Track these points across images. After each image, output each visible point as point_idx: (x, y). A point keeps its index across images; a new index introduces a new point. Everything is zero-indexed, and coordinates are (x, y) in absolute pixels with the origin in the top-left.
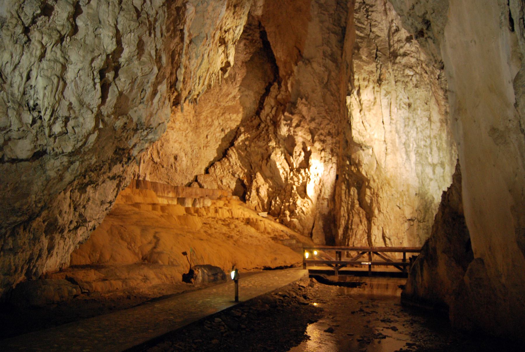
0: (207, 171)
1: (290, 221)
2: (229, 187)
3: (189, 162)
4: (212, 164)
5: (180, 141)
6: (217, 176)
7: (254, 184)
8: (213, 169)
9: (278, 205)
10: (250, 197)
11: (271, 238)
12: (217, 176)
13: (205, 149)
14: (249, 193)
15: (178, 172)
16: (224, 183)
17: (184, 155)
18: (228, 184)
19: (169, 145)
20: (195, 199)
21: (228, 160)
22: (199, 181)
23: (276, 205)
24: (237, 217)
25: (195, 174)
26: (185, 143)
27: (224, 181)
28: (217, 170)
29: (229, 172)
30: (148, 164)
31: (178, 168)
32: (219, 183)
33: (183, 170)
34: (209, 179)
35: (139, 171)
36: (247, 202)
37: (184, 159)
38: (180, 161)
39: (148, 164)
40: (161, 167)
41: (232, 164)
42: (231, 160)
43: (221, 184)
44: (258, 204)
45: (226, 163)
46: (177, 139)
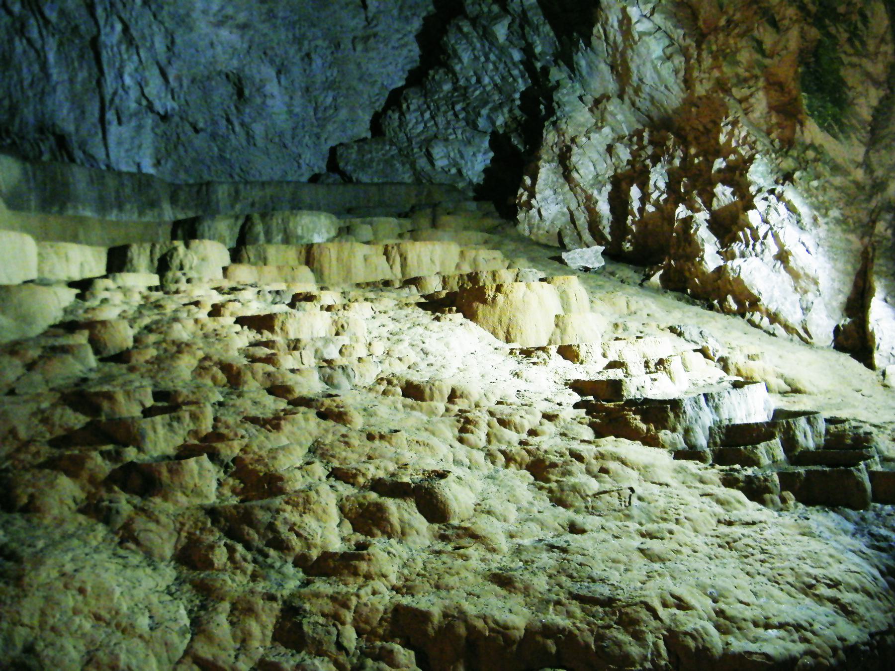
0: (377, 126)
1: (720, 270)
2: (460, 172)
3: (298, 101)
4: (395, 99)
5: (242, 18)
6: (409, 140)
7: (550, 137)
8: (396, 116)
9: (656, 204)
10: (532, 195)
11: (577, 386)
12: (409, 140)
13: (359, 47)
14: (528, 181)
15: (260, 142)
16: (440, 163)
17: (269, 72)
18: (455, 164)
19: (194, 35)
20: (248, 218)
21: (450, 70)
22: (341, 165)
23: (650, 208)
24: (772, 308)
25: (332, 143)
26: (265, 28)
27: (438, 151)
28: (412, 118)
29: (456, 115)
30: (139, 128)
31: (258, 129)
32: (422, 162)
33: (281, 134)
34: (379, 152)
35: (108, 155)
36: (521, 216)
37: (272, 87)
38: (258, 100)
39: (139, 128)
40: (188, 128)
41: (462, 82)
42: (458, 68)
43: (428, 168)
44: (573, 220)
45: (439, 84)
46: (230, 11)
